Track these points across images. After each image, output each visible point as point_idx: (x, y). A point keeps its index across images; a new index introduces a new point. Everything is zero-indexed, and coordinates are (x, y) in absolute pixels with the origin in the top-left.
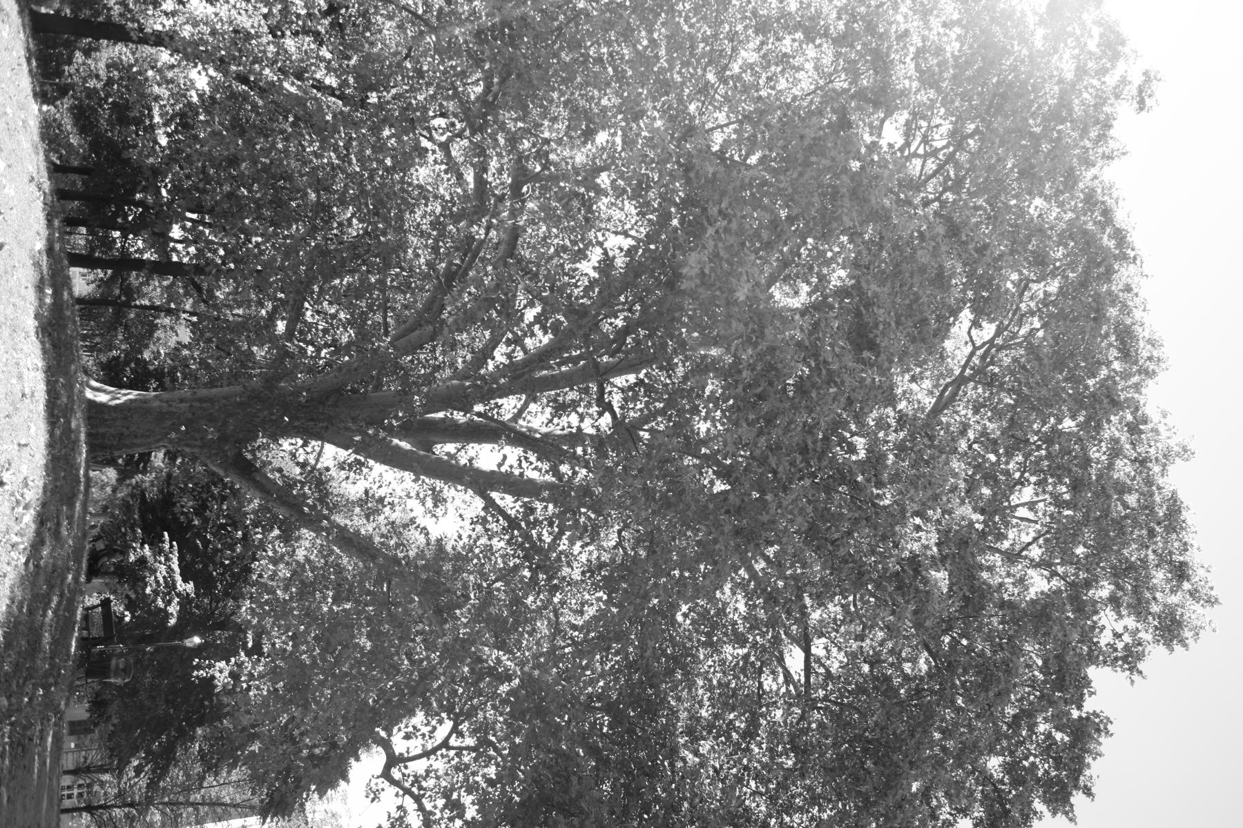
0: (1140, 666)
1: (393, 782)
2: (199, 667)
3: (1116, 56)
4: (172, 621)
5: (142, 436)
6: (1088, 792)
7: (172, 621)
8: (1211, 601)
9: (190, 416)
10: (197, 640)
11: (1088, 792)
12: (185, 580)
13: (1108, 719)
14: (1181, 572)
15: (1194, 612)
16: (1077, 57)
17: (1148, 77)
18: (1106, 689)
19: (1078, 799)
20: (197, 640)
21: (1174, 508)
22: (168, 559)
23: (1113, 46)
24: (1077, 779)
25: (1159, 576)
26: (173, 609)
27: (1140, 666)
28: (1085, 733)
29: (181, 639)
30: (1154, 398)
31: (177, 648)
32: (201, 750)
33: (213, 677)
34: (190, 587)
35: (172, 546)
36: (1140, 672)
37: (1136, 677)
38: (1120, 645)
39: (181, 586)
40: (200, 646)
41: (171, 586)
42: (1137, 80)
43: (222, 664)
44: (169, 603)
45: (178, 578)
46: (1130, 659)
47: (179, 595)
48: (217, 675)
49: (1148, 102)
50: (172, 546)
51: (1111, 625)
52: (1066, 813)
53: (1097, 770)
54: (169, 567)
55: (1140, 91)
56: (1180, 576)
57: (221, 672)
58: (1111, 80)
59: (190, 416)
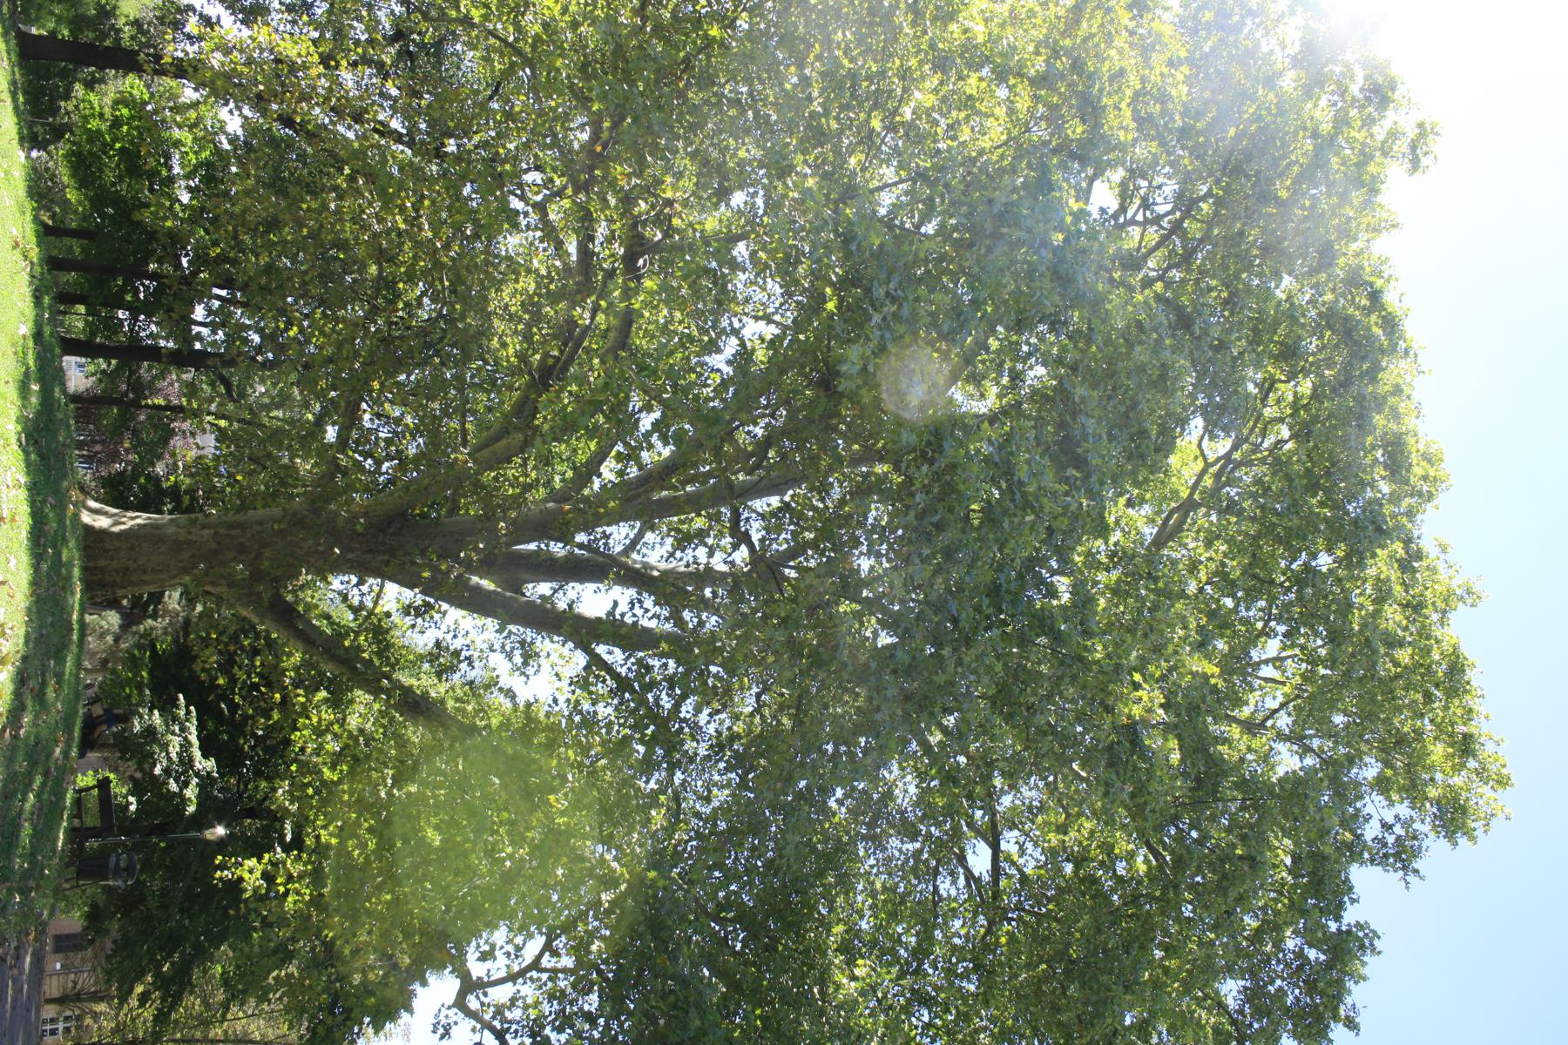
2: (222, 867)
4: (191, 809)
5: (153, 571)
6: (1351, 1024)
7: (191, 809)
8: (1503, 782)
9: (214, 545)
11: (1351, 1024)
12: (205, 756)
13: (1375, 933)
14: (1465, 747)
15: (1483, 797)
18: (1372, 894)
24: (1336, 1008)
26: (191, 793)
28: (1347, 949)
33: (241, 879)
34: (210, 764)
36: (1416, 871)
38: (1391, 839)
41: (186, 762)
42: (1412, 133)
43: (251, 862)
45: (197, 754)
47: (197, 774)
48: (246, 876)
49: (1424, 161)
50: (188, 712)
51: (1379, 813)
54: (186, 739)
57: (250, 872)
58: (1380, 132)
59: (214, 545)
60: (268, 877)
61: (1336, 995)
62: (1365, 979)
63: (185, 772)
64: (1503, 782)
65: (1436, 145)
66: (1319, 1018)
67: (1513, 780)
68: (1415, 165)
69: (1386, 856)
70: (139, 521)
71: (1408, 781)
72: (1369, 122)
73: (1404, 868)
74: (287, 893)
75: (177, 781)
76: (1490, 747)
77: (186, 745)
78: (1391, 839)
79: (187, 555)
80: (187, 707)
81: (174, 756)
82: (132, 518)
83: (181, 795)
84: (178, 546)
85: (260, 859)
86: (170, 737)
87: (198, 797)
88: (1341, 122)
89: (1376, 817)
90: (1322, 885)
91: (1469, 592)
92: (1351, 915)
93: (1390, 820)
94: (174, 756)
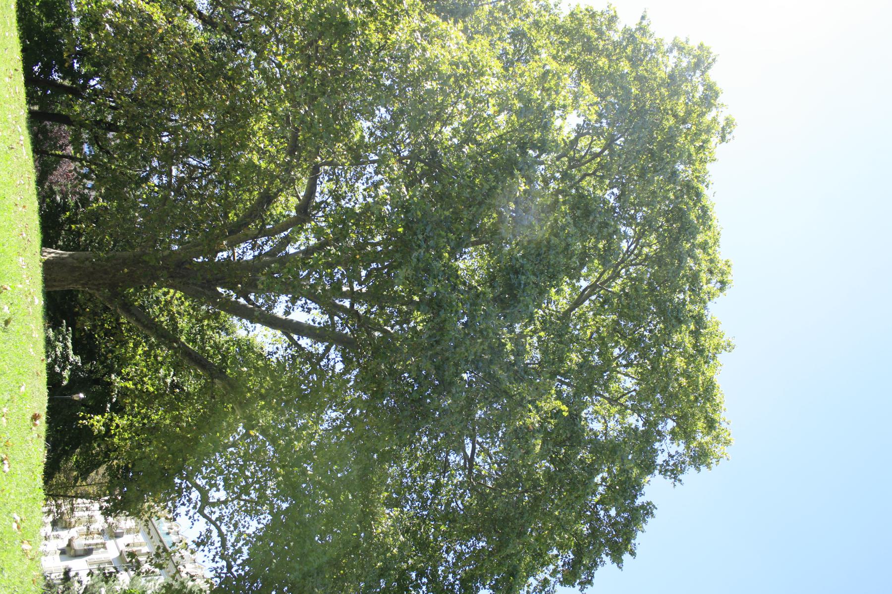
0: (680, 477)
1: (205, 516)
2: (83, 418)
3: (710, 106)
4: (65, 383)
5: (59, 281)
6: (633, 553)
7: (65, 383)
8: (727, 443)
9: (91, 270)
10: (82, 395)
11: (633, 553)
12: (75, 354)
13: (654, 506)
14: (711, 424)
15: (718, 449)
16: (687, 104)
17: (729, 123)
18: (654, 489)
19: (626, 557)
20: (82, 395)
21: (710, 387)
22: (65, 339)
23: (709, 98)
24: (627, 545)
25: (701, 424)
26: (66, 374)
27: (680, 477)
28: (638, 515)
29: (71, 394)
30: (719, 311)
31: (66, 400)
32: (77, 461)
33: (92, 425)
34: (78, 358)
35: (67, 330)
36: (680, 481)
37: (677, 483)
38: (671, 463)
39: (73, 358)
40: (83, 399)
41: (65, 357)
42: (723, 123)
43: (99, 417)
44: (63, 369)
45: (71, 352)
46: (673, 471)
47: (71, 364)
48: (95, 423)
49: (728, 136)
50: (67, 330)
51: (667, 449)
52: (618, 564)
53: (641, 540)
54: (65, 344)
55: (723, 129)
56: (710, 427)
57: (97, 422)
58: (708, 118)
59: (91, 270)
60: (107, 426)
61: (628, 537)
62: (700, 470)
63: (64, 362)
64: (727, 443)
65: (736, 131)
66: (619, 549)
67: (733, 443)
68: (723, 138)
69: (666, 471)
70: (53, 255)
71: (684, 432)
72: (702, 114)
73: (675, 478)
74: (115, 434)
75: (59, 366)
76: (724, 425)
77: (65, 347)
78: (671, 463)
79: (77, 274)
80: (67, 327)
81: (58, 353)
82: (50, 253)
83: (60, 374)
84: (73, 269)
85: (103, 416)
86: (57, 343)
87: (70, 376)
88: (689, 113)
89: (666, 451)
90: (625, 490)
91: (729, 345)
92: (639, 501)
93: (673, 453)
94: (58, 353)
